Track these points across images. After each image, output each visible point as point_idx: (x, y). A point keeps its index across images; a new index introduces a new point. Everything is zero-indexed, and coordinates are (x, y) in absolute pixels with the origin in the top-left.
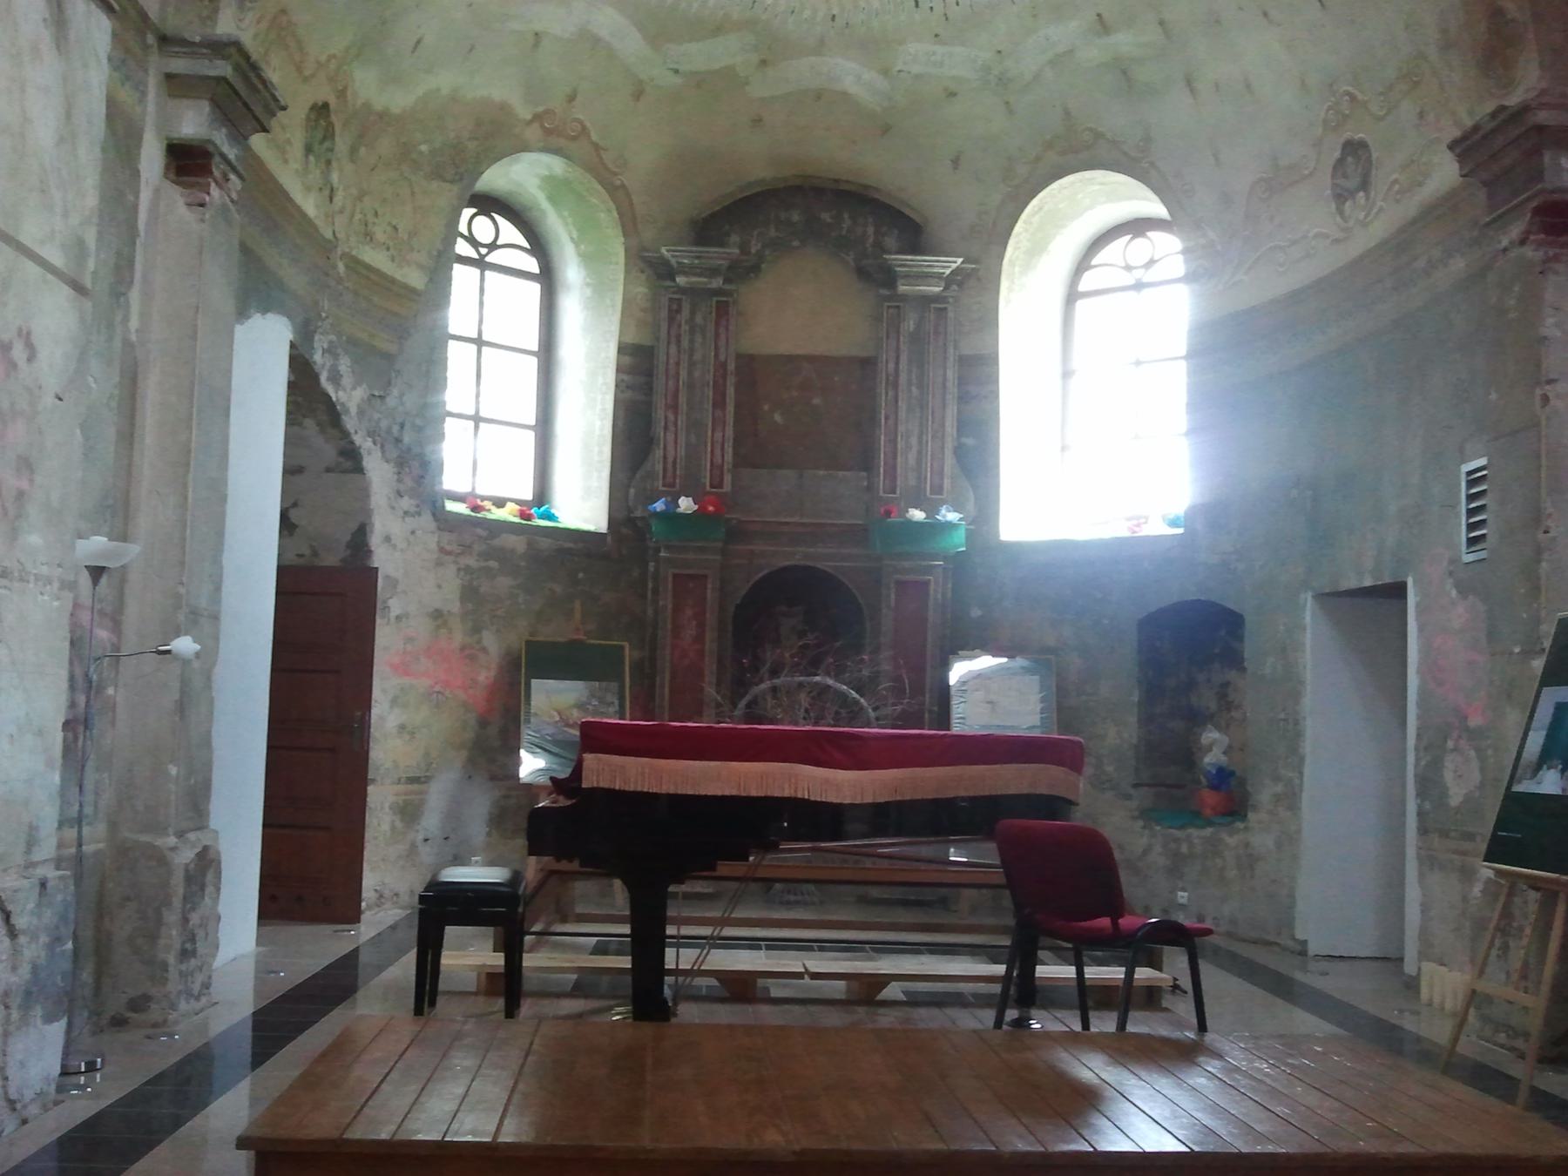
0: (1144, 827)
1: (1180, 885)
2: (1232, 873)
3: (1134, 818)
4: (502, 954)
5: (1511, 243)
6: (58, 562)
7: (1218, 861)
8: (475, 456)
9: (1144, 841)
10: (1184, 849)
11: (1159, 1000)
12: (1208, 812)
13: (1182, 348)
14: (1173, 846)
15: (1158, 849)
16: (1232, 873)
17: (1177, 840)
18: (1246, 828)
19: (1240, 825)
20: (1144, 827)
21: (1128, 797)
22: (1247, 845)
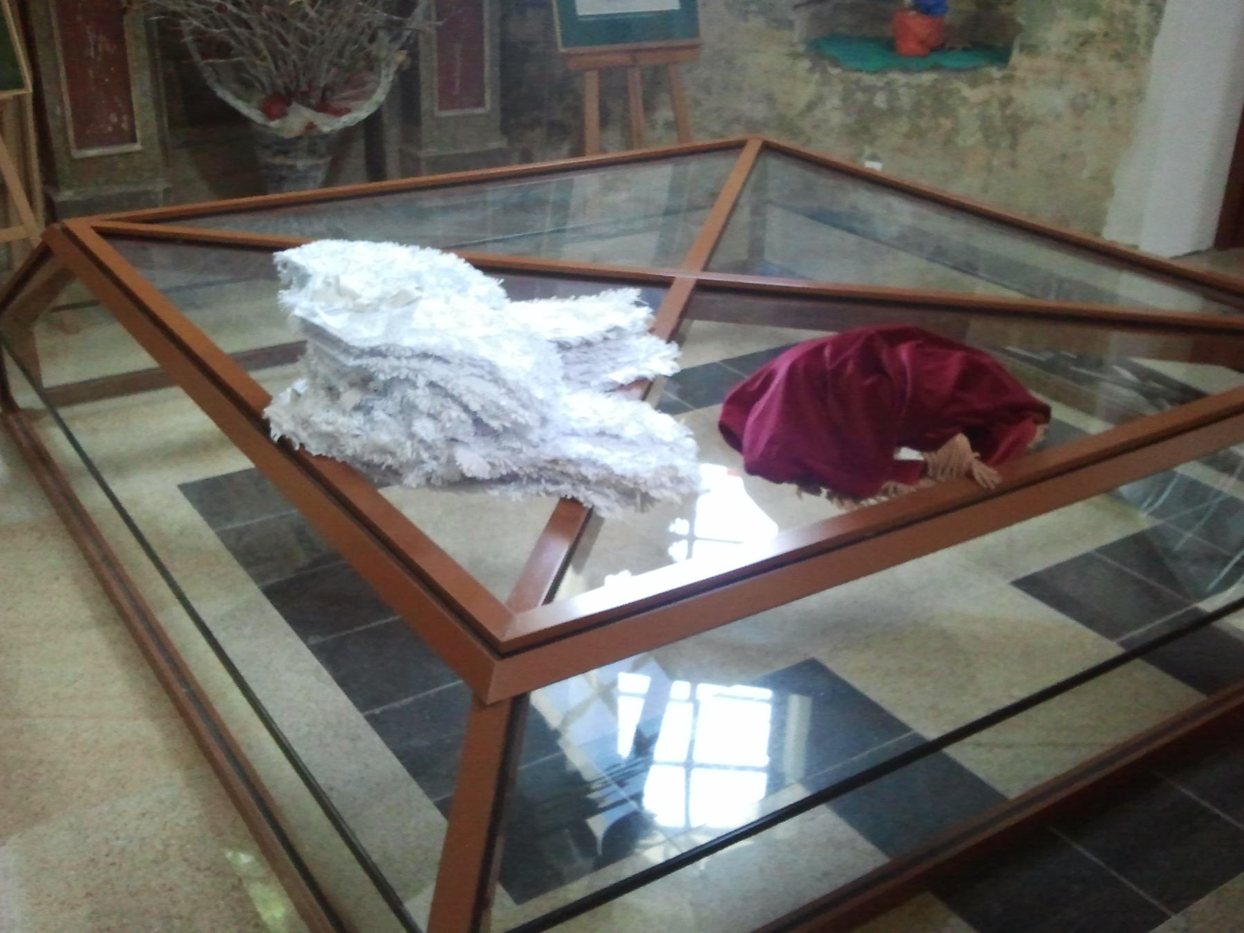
0: (811, 70)
1: (868, 150)
2: (970, 138)
3: (795, 56)
4: (580, 13)
5: (475, 413)
6: (521, 465)
7: (947, 123)
8: (693, 735)
9: (805, 94)
10: (880, 101)
11: (41, 244)
12: (911, 46)
13: (653, 769)
14: (860, 97)
15: (835, 101)
16: (970, 138)
17: (870, 90)
18: (1008, 79)
19: (995, 72)
20: (811, 70)
21: (790, 25)
22: (1006, 102)
